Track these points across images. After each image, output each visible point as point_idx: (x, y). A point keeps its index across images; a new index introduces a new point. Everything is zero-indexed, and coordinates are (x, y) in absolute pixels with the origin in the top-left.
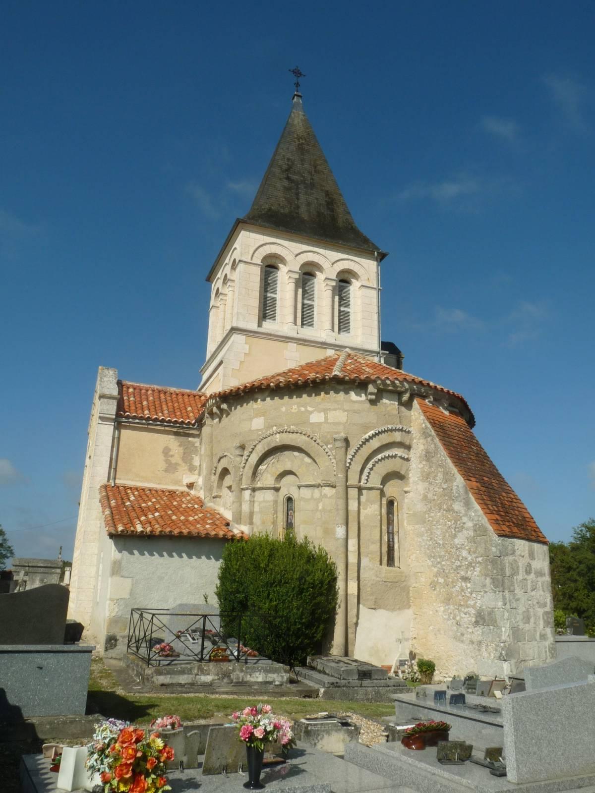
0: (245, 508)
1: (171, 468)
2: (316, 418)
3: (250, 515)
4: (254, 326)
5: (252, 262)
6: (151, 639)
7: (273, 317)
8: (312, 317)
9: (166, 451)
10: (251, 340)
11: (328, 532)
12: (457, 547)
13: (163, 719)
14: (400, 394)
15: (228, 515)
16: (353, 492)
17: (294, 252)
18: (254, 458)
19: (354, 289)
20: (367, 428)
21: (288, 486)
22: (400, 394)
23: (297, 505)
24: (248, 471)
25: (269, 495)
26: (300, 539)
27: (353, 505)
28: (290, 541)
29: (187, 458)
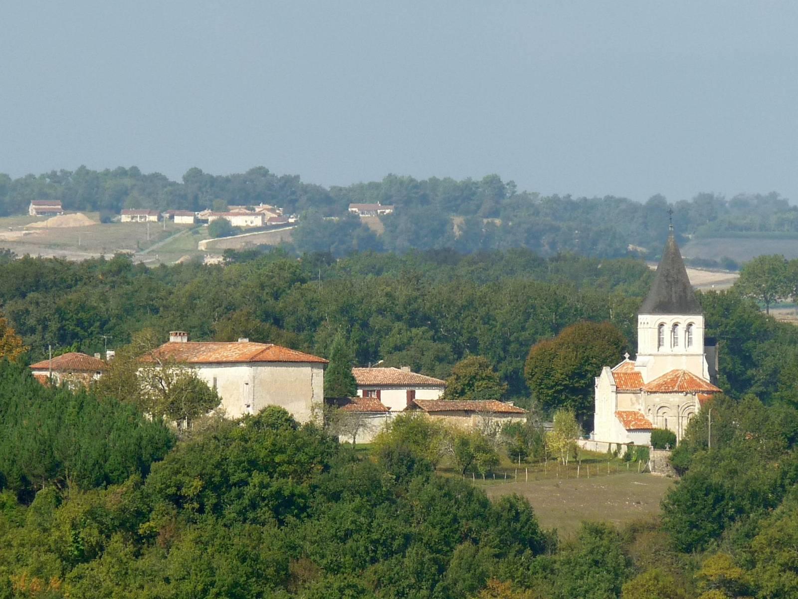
0: (656, 421)
1: (633, 404)
2: (671, 400)
3: (658, 423)
4: (655, 351)
5: (660, 353)
6: (465, 471)
7: (663, 345)
8: (677, 342)
9: (631, 399)
10: (655, 357)
11: (675, 428)
12: (57, 286)
13: (513, 515)
14: (692, 393)
15: (651, 421)
16: (680, 418)
17: (669, 319)
18: (657, 409)
19: (693, 328)
20: (684, 402)
21: (666, 416)
22: (692, 393)
23: (668, 420)
24: (656, 411)
25: (661, 418)
26: (669, 429)
27: (680, 421)
28: (666, 429)
29: (637, 400)
